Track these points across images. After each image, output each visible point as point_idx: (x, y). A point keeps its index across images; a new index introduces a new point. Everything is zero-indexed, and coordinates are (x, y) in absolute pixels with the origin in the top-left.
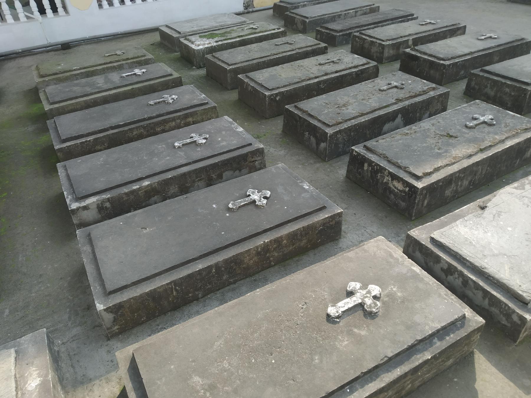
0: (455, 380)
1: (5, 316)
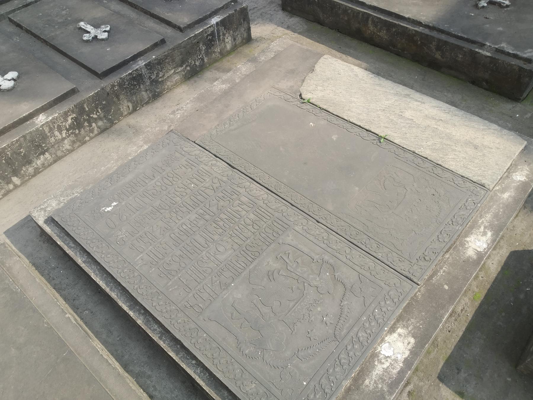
0: (446, 287)
1: (525, 117)
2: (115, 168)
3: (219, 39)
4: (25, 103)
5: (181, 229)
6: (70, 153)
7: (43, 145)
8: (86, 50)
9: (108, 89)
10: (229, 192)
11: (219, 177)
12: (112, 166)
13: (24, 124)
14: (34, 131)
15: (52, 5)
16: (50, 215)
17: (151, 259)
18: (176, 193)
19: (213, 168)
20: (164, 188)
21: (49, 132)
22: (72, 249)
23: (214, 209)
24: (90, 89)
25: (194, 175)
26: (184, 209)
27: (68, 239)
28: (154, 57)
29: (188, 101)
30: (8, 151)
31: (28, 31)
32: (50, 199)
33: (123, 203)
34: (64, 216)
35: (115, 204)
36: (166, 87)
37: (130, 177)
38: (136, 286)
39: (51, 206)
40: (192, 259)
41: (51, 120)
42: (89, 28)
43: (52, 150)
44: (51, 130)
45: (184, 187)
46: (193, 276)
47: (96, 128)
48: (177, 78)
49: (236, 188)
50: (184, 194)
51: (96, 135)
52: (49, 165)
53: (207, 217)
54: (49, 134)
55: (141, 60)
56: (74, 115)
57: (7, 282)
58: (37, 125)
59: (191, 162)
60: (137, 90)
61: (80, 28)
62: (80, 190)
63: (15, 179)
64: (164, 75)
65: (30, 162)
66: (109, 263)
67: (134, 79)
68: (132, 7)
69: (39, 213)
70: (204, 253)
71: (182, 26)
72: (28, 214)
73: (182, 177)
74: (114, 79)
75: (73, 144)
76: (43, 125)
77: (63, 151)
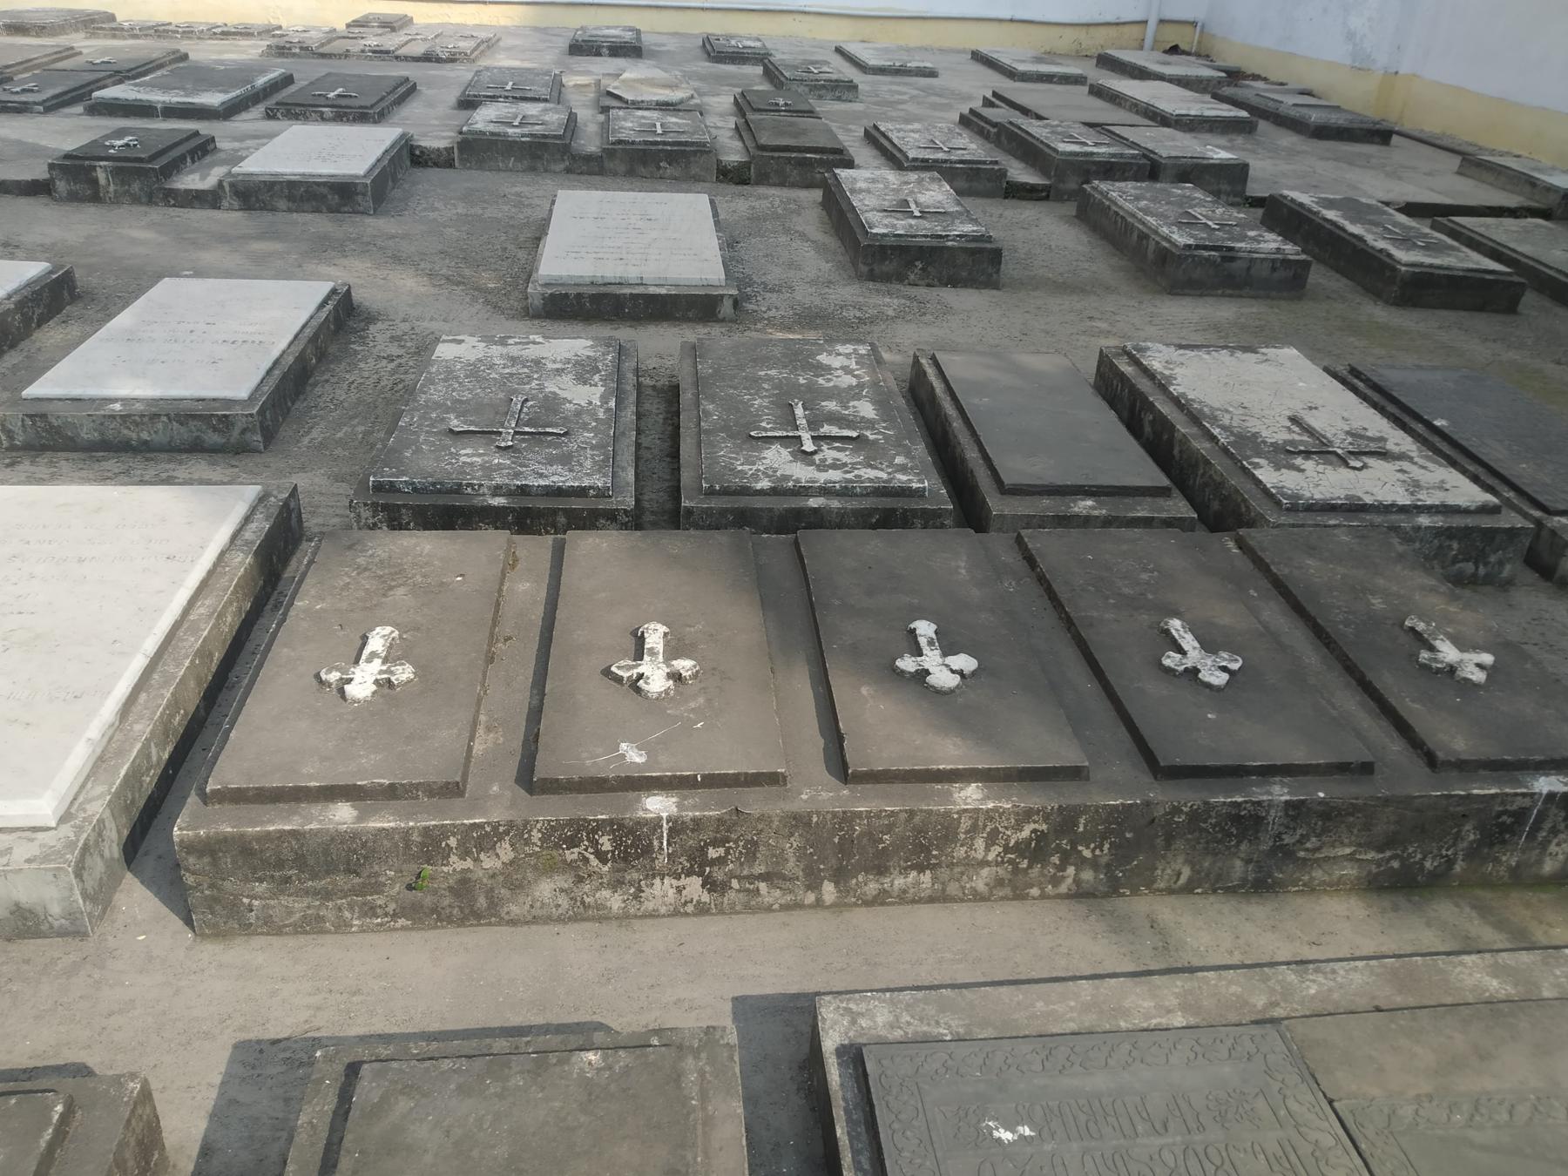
3: (1532, 836)
4: (958, 741)
6: (975, 900)
8: (1155, 688)
9: (1159, 812)
13: (928, 786)
14: (938, 813)
15: (1125, 547)
16: (861, 1040)
21: (967, 832)
24: (1118, 788)
27: (864, 1137)
28: (1321, 795)
31: (1042, 580)
33: (1048, 1147)
34: (889, 1073)
35: (1027, 1131)
36: (1306, 878)
37: (1099, 1082)
39: (872, 1018)
41: (988, 811)
42: (1188, 642)
43: (944, 873)
44: (974, 830)
47: (1070, 880)
48: (1350, 871)
52: (913, 902)
55: (1283, 785)
56: (1045, 827)
57: (689, 1156)
58: (954, 803)
60: (1228, 848)
61: (1167, 632)
63: (829, 891)
64: (1318, 849)
65: (881, 871)
67: (1236, 819)
71: (1441, 755)
74: (1188, 796)
76: (966, 811)
77: (963, 888)
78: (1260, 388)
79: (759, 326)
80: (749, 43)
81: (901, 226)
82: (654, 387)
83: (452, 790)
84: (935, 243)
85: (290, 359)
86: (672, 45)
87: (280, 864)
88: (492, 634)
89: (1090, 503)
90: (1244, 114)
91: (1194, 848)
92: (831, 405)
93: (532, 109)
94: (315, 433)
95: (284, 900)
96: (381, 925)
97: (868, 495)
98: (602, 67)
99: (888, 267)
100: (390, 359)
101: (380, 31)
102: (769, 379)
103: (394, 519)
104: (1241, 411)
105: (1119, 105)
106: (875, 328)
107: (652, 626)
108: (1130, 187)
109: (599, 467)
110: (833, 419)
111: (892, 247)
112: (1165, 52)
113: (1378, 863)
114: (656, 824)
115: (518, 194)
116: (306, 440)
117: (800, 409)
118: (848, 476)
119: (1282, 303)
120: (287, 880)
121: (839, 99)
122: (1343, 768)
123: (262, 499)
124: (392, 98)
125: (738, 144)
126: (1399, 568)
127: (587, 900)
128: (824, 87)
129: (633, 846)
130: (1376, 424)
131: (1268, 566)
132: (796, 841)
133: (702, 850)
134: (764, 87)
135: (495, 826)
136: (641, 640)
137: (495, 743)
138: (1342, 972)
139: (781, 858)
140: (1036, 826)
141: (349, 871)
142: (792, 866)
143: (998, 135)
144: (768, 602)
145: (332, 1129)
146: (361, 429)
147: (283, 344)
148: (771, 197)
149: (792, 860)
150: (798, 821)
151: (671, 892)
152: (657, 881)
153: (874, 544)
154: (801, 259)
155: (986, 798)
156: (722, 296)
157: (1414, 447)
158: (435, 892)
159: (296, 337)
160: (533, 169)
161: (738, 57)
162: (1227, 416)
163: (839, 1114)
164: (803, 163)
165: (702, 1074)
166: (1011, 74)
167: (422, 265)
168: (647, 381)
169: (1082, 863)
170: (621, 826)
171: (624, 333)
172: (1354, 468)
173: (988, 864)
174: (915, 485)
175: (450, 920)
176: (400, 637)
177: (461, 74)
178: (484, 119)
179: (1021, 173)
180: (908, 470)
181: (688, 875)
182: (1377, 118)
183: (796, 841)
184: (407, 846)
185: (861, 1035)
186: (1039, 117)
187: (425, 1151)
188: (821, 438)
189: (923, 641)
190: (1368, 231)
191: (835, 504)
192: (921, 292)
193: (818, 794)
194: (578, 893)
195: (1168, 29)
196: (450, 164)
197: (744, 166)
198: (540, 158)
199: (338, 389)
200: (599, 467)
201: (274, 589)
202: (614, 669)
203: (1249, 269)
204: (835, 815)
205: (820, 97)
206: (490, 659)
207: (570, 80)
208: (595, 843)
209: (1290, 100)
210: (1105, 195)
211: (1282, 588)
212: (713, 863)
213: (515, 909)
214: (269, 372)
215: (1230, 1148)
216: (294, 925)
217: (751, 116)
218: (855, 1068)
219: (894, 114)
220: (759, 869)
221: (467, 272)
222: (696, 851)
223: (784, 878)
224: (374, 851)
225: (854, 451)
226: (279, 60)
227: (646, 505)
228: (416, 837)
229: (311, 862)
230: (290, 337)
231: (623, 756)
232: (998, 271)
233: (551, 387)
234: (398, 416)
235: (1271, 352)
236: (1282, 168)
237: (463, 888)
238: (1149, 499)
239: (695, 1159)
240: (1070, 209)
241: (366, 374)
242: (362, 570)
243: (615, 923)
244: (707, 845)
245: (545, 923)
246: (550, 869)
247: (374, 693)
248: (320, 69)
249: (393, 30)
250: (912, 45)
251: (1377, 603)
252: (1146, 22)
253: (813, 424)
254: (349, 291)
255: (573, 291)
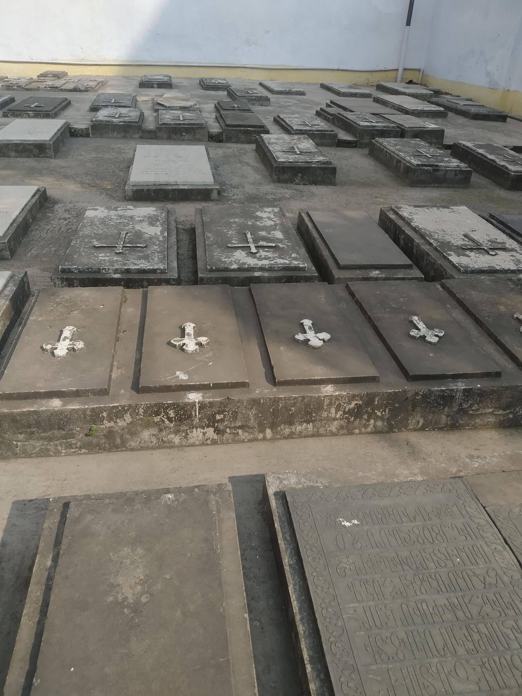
2: (375, 481)
4: (323, 367)
5: (420, 607)
7: (314, 415)
8: (408, 345)
9: (409, 395)
10: (506, 601)
11: (500, 572)
12: (372, 477)
13: (310, 386)
14: (315, 397)
15: (393, 288)
16: (284, 489)
17: (365, 618)
18: (433, 555)
19: (495, 554)
20: (421, 541)
21: (327, 406)
22: (286, 542)
23: (475, 610)
24: (393, 384)
25: (466, 549)
26: (434, 584)
27: (287, 527)
28: (479, 386)
29: (496, 454)
30: (281, 403)
32: (292, 473)
33: (365, 528)
35: (356, 522)
36: (473, 423)
37: (386, 502)
38: (332, 639)
40: (416, 657)
41: (336, 396)
42: (421, 325)
43: (318, 424)
44: (330, 404)
45: (446, 554)
46: (407, 681)
47: (372, 426)
48: (492, 419)
49: (517, 602)
50: (443, 564)
51: (367, 433)
52: (305, 437)
53: (460, 614)
54: (326, 407)
55: (462, 382)
56: (361, 402)
57: (213, 533)
58: (322, 393)
59: (469, 529)
60: (439, 410)
61: (412, 322)
62: (325, 482)
63: (268, 432)
64: (477, 410)
66: (317, 586)
67: (443, 397)
68: (477, 323)
69: (274, 480)
70: (436, 660)
72: (261, 472)
73: (449, 541)
74: (422, 388)
75: (340, 429)
76: (327, 396)
77: (326, 430)
78: (449, 223)
79: (229, 202)
80: (220, 81)
81: (291, 158)
82: (184, 229)
83: (103, 392)
84: (307, 165)
85: (21, 219)
86: (185, 83)
87: (29, 426)
88: (117, 330)
89: (377, 272)
90: (442, 109)
91: (425, 411)
92: (263, 233)
93: (124, 111)
94: (33, 252)
95: (32, 442)
96: (74, 452)
97: (280, 270)
98: (154, 93)
99: (286, 176)
100: (65, 219)
101: (53, 78)
102: (235, 223)
103: (70, 283)
104: (443, 232)
105: (387, 106)
106: (281, 203)
107: (188, 324)
108: (392, 140)
109: (161, 261)
110: (264, 239)
111: (288, 168)
112: (407, 83)
113: (504, 416)
114: (193, 405)
115: (119, 148)
116: (29, 254)
117: (249, 236)
118: (272, 262)
119: (460, 189)
120: (33, 433)
121: (262, 105)
122: (488, 375)
123: (11, 277)
124: (60, 107)
125: (217, 125)
126: (511, 294)
127: (164, 439)
128: (254, 99)
129: (183, 415)
130: (501, 237)
131: (455, 294)
132: (254, 411)
133: (214, 416)
134: (228, 100)
135: (123, 407)
136: (183, 330)
137: (121, 373)
138: (488, 458)
139: (248, 419)
140: (357, 402)
141: (59, 428)
142: (252, 422)
143: (333, 119)
144: (239, 314)
145: (59, 529)
146: (53, 249)
147: (17, 213)
148: (233, 148)
149: (253, 419)
150: (255, 402)
151: (201, 435)
152: (194, 430)
153: (284, 289)
154: (247, 174)
155: (335, 391)
156: (212, 189)
157: (518, 246)
158: (98, 437)
159: (23, 209)
160: (125, 137)
161: (216, 88)
162: (437, 235)
163: (276, 518)
164: (247, 132)
165: (217, 502)
166: (338, 93)
167: (77, 179)
168: (181, 227)
169: (377, 418)
170: (178, 406)
171: (170, 206)
172: (492, 255)
173: (337, 419)
174: (301, 266)
175: (104, 449)
176: (77, 331)
177: (91, 97)
178: (102, 115)
179: (343, 136)
180: (299, 259)
181: (208, 427)
182: (501, 110)
183: (254, 411)
184: (85, 417)
185: (284, 487)
186: (351, 111)
187: (100, 535)
188: (259, 240)
189: (306, 328)
190: (497, 158)
191: (266, 274)
192: (301, 187)
193: (263, 390)
194: (160, 436)
195: (408, 72)
196: (87, 136)
197: (220, 134)
198: (128, 132)
199: (42, 232)
200: (161, 261)
201: (19, 316)
202: (172, 341)
203: (445, 174)
204: (270, 399)
205: (253, 104)
206: (117, 339)
207: (140, 99)
208: (167, 414)
209: (462, 103)
210: (381, 144)
211: (461, 303)
212: (218, 421)
213: (133, 444)
214: (11, 224)
215: (442, 526)
216: (36, 453)
217: (222, 112)
218: (282, 501)
219: (286, 111)
220: (239, 424)
221: (98, 182)
222: (211, 416)
223: (249, 427)
224: (70, 419)
225: (274, 252)
226: (7, 92)
227: (182, 278)
228: (88, 413)
229: (43, 424)
230: (20, 210)
231: (178, 377)
232: (335, 178)
233: (138, 227)
234: (71, 241)
235: (455, 208)
236: (458, 132)
237: (110, 434)
238: (403, 270)
239: (216, 534)
240: (366, 151)
241: (55, 226)
242: (58, 304)
243: (176, 449)
244: (215, 413)
245: (146, 450)
246: (148, 425)
247: (67, 353)
248: (26, 95)
249: (59, 78)
250: (293, 82)
251: (502, 308)
252: (398, 70)
253: (255, 241)
254: (45, 190)
255: (145, 188)
